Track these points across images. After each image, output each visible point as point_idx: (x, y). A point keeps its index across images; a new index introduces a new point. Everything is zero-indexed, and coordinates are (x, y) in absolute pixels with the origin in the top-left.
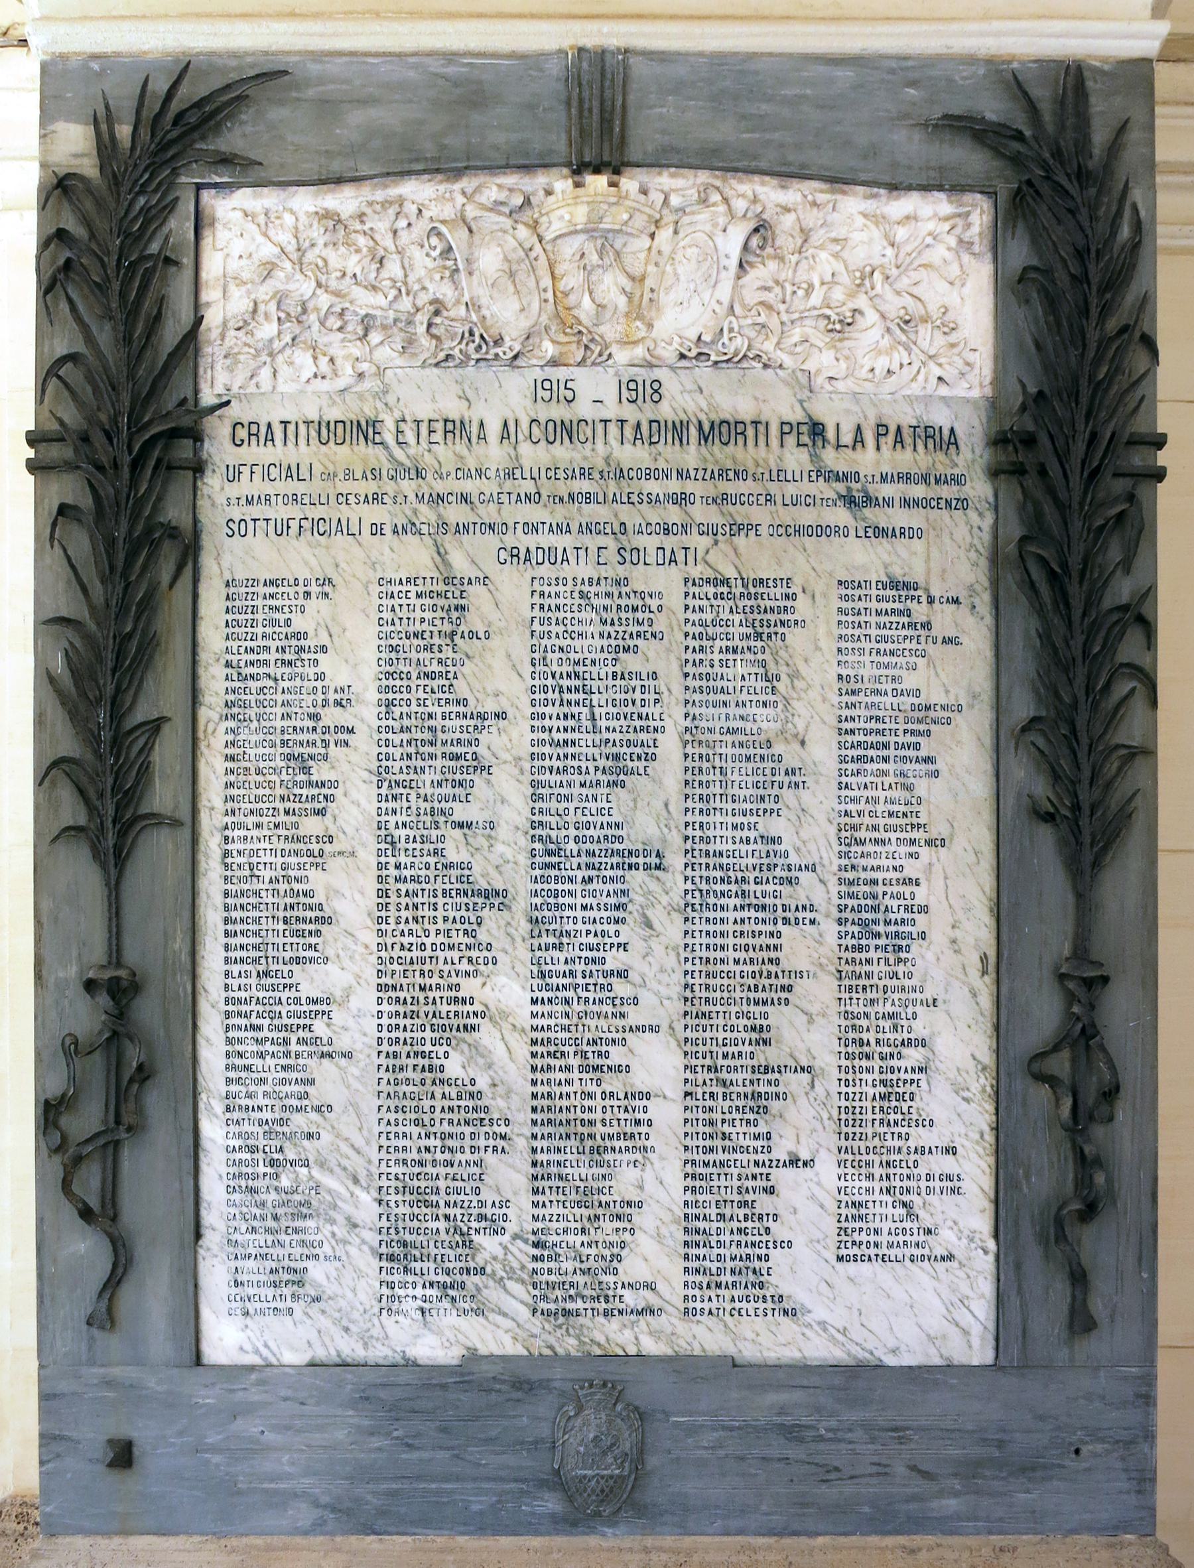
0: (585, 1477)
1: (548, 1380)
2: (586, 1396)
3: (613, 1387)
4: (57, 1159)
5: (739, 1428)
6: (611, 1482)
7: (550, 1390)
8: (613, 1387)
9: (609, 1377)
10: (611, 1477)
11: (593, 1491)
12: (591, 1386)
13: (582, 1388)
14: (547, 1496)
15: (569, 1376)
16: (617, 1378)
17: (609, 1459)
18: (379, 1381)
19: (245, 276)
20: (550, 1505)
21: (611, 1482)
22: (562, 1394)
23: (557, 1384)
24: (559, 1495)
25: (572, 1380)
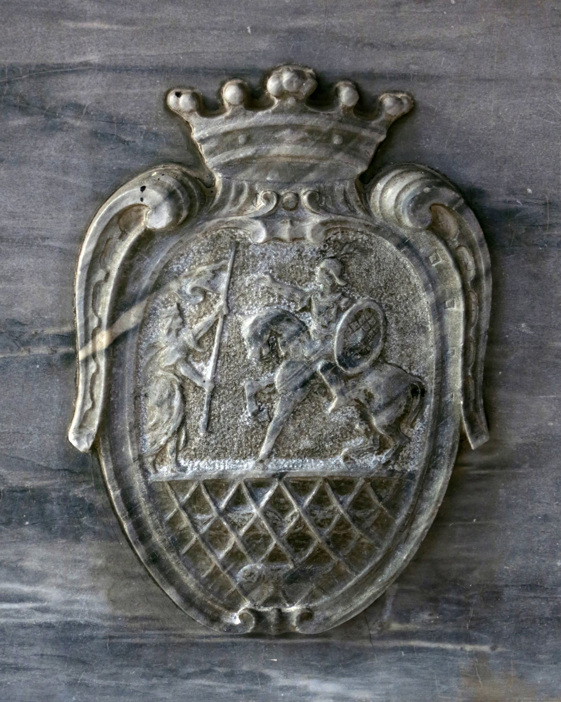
0: (216, 486)
1: (44, 72)
2: (227, 141)
3: (365, 107)
4: (152, 341)
5: (184, 399)
6: (338, 507)
7: (50, 118)
8: (365, 107)
9: (344, 61)
10: (340, 485)
11: (254, 541)
12: (253, 99)
13: (208, 107)
14: (35, 556)
15: (149, 53)
16: (386, 62)
17: (334, 407)
18: (497, 471)
19: (255, 408)
20: (52, 594)
21: (338, 507)
22: (110, 130)
23: (86, 90)
24: (91, 552)
25: (160, 70)
